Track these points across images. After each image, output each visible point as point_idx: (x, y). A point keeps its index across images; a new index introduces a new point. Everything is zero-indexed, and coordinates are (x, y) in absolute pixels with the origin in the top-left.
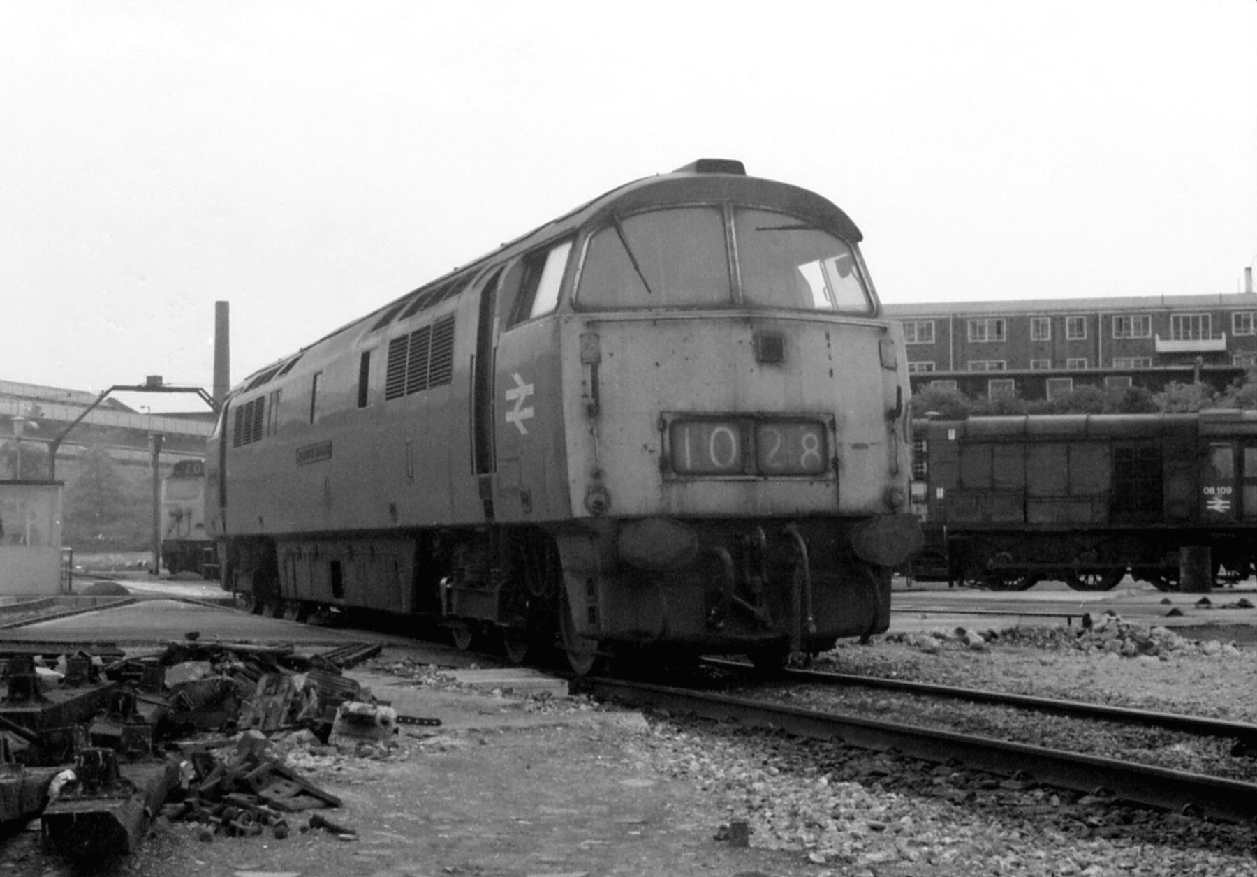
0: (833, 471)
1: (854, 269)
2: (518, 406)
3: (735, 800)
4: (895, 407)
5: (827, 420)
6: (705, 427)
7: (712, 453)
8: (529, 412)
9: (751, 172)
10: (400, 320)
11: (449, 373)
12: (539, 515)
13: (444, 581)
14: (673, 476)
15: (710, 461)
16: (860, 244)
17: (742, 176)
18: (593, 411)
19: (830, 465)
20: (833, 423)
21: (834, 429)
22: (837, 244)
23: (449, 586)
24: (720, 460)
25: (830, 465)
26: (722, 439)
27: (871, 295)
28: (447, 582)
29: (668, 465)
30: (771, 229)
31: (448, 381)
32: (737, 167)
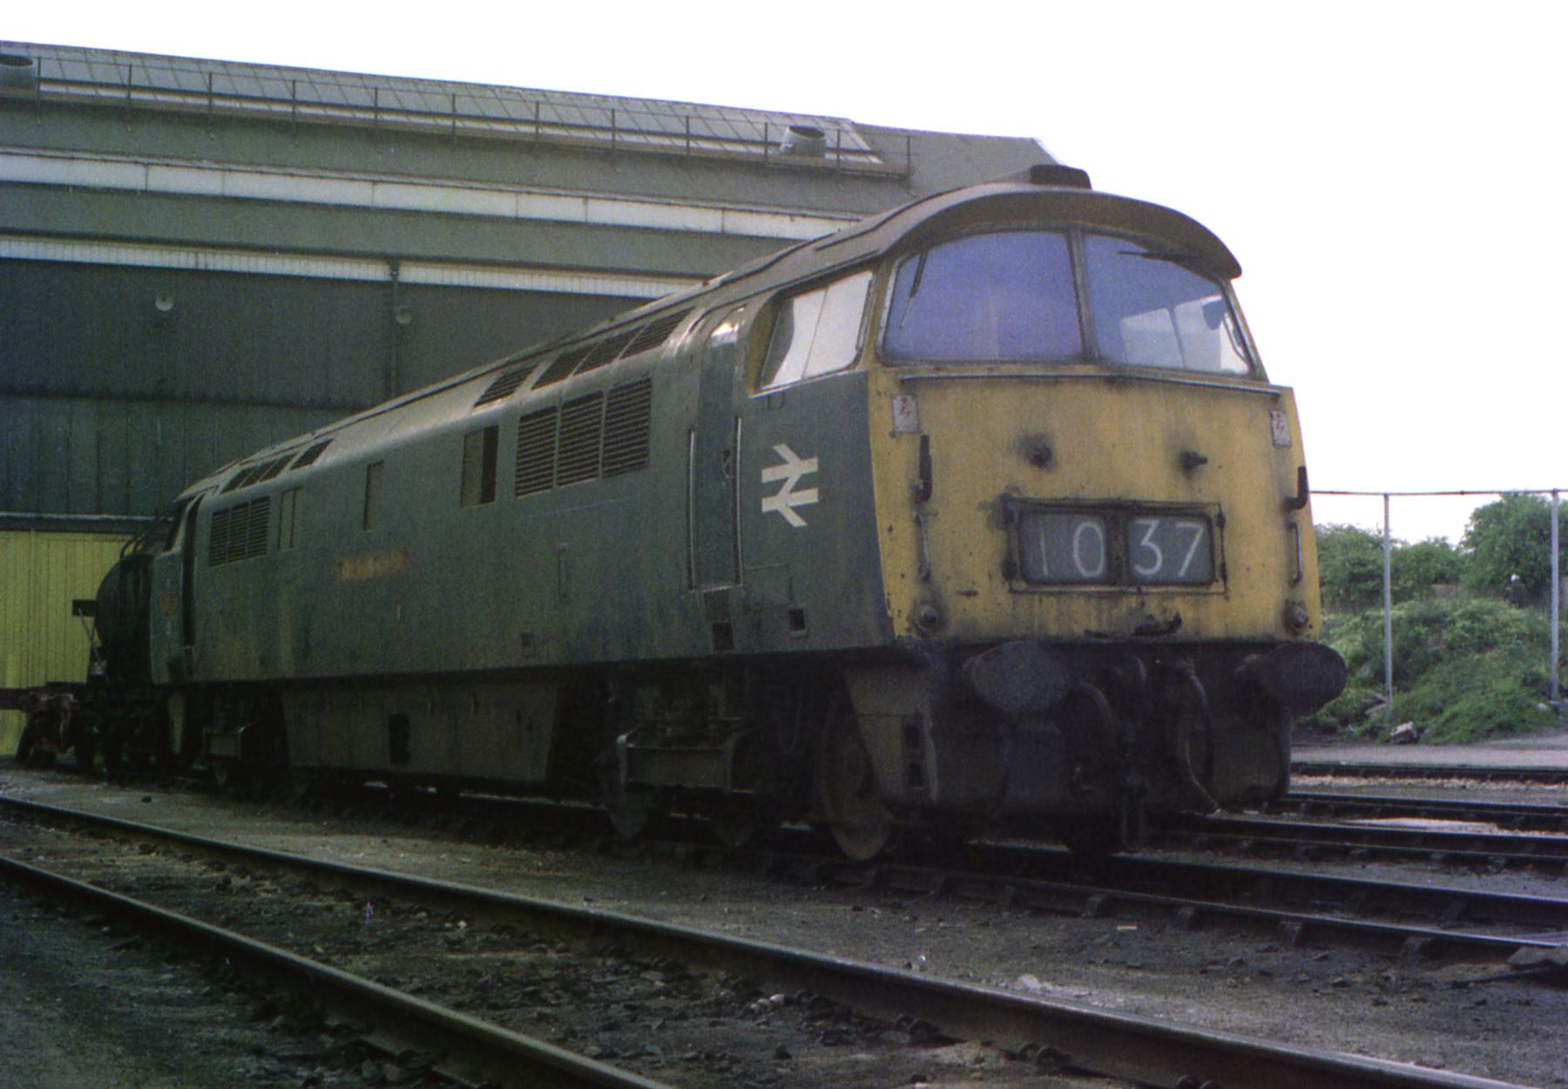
0: (1221, 582)
1: (1229, 321)
2: (790, 484)
3: (113, 1012)
4: (1295, 495)
5: (1213, 512)
7: (1076, 556)
8: (810, 496)
9: (1099, 185)
10: (293, 468)
11: (645, 453)
12: (817, 639)
13: (623, 738)
14: (1022, 585)
15: (1072, 566)
16: (1235, 283)
17: (1083, 190)
18: (922, 494)
19: (1217, 573)
20: (1221, 521)
22: (1213, 286)
23: (631, 745)
25: (1217, 573)
26: (1089, 533)
27: (1251, 351)
28: (629, 739)
29: (1013, 569)
30: (368, 482)
31: (642, 466)
32: (1080, 178)
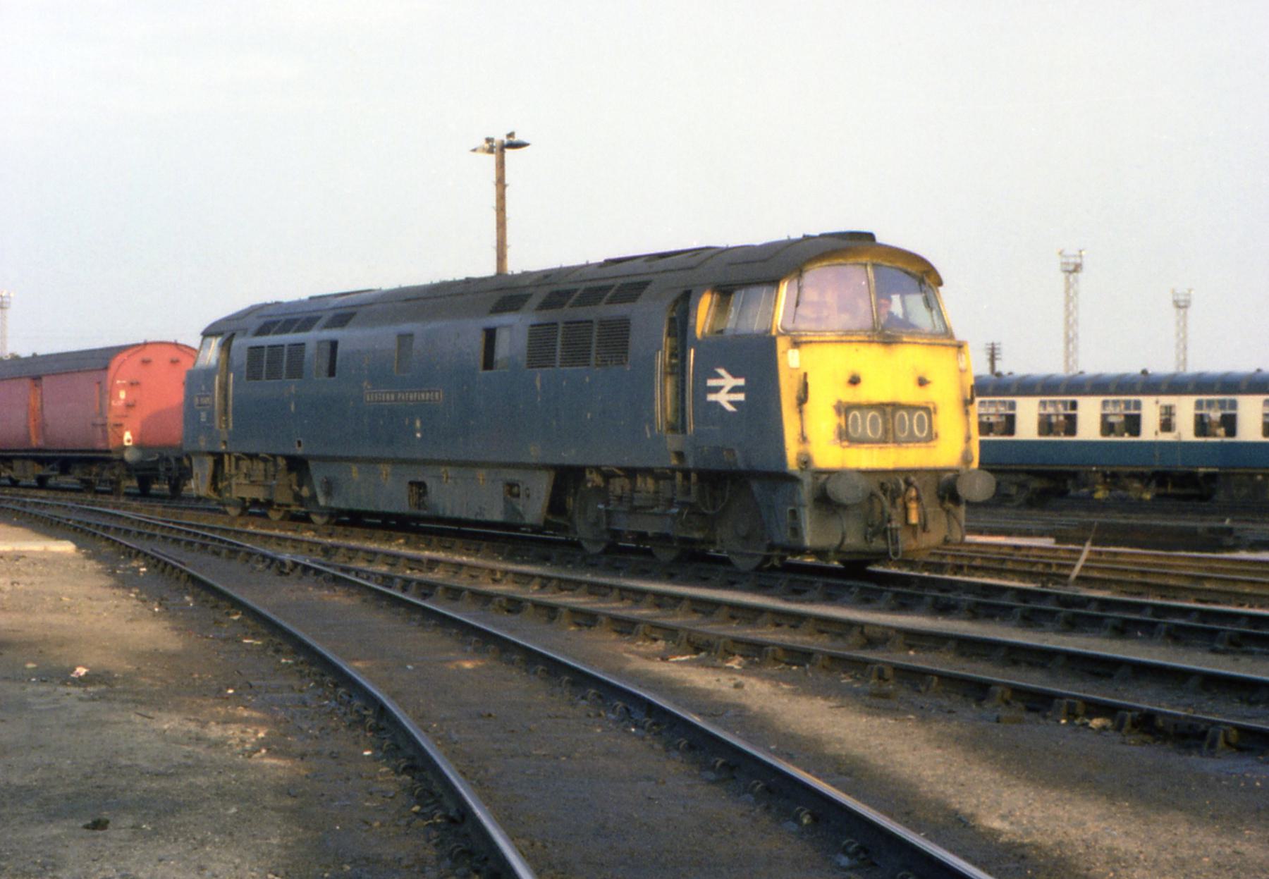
5: (931, 407)
6: (865, 411)
20: (935, 409)
21: (935, 412)
24: (872, 432)
32: (870, 237)
